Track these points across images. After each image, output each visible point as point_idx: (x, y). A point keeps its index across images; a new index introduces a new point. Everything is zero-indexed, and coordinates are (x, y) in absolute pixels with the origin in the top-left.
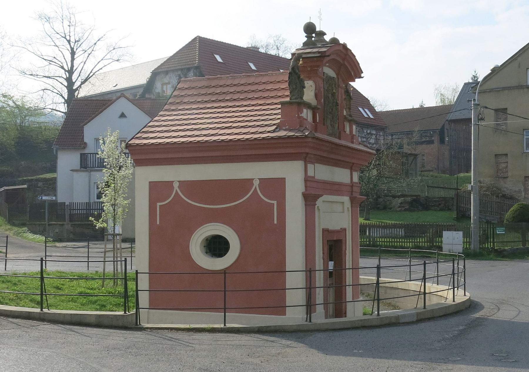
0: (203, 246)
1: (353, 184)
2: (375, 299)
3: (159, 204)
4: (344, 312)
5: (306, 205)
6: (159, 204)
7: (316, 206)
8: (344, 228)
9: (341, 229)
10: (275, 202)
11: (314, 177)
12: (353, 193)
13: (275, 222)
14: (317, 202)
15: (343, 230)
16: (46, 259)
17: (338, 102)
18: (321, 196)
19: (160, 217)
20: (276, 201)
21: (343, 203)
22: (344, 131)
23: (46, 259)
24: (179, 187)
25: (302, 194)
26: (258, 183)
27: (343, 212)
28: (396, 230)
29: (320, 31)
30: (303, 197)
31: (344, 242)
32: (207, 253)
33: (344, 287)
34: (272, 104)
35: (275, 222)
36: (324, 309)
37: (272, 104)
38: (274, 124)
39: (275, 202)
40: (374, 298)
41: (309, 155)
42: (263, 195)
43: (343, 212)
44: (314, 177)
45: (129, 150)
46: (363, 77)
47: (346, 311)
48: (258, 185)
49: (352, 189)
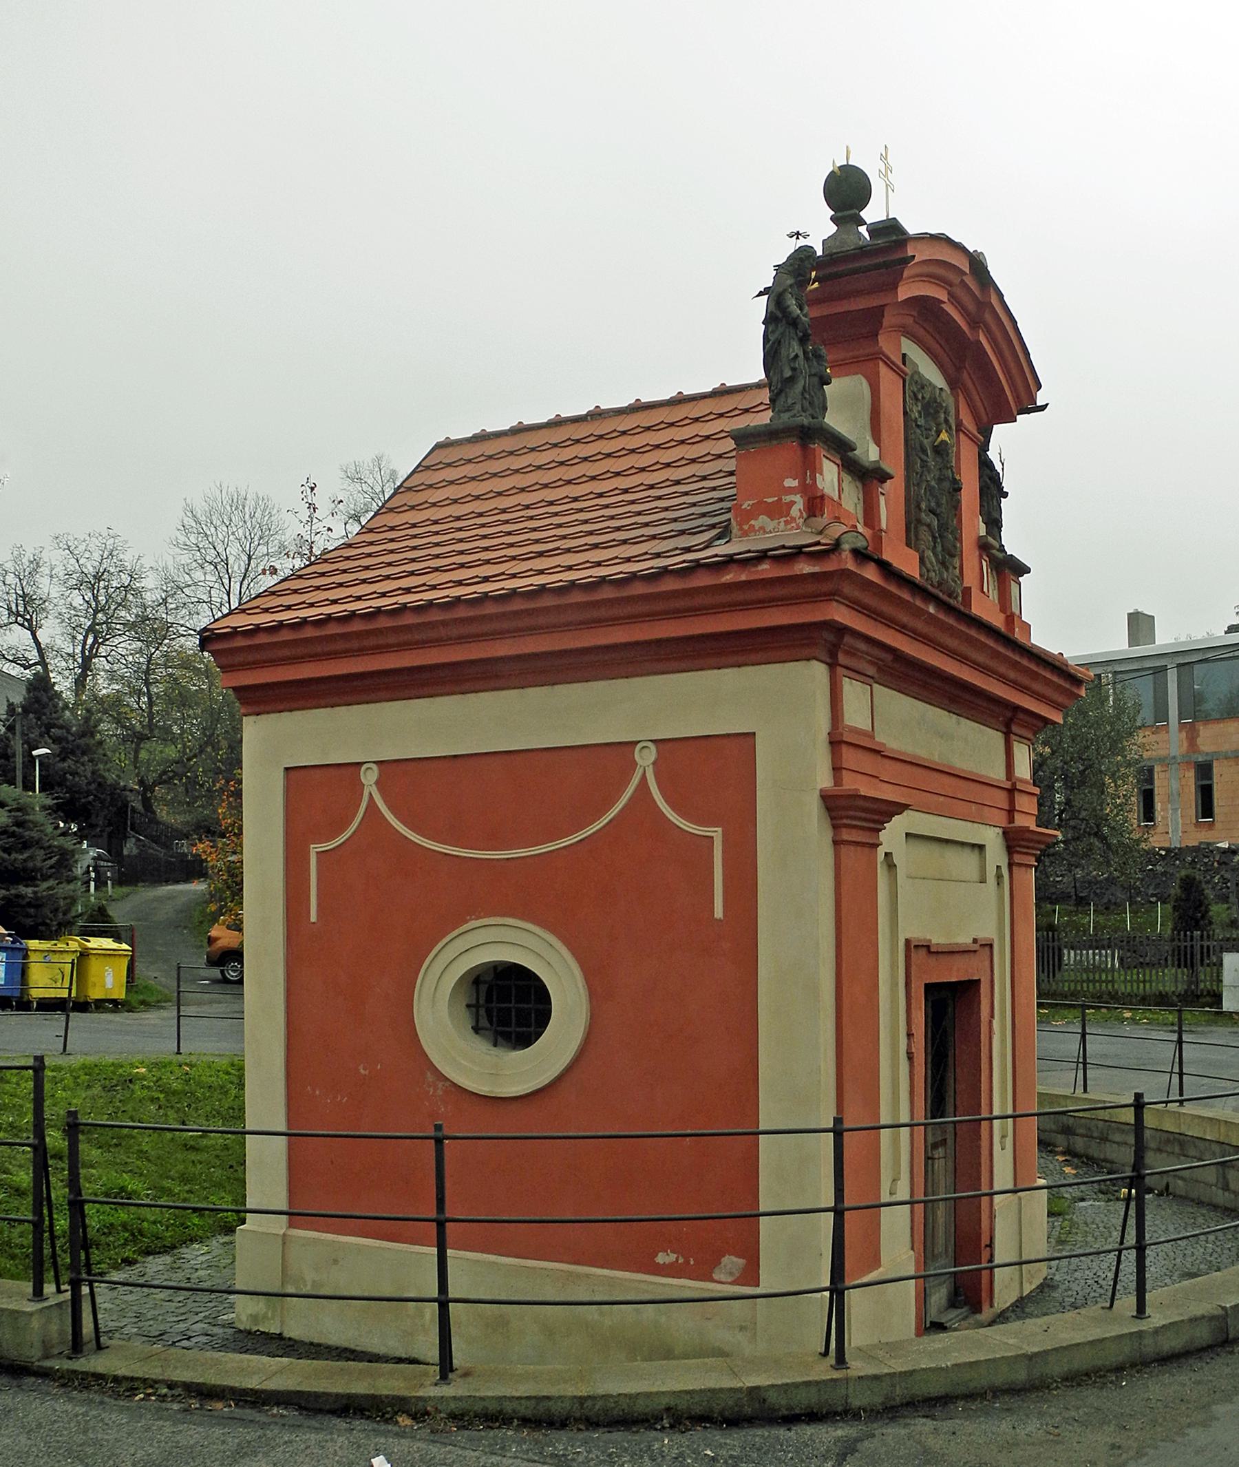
0: (464, 1004)
1: (1014, 784)
2: (1126, 1244)
3: (315, 849)
4: (985, 1240)
5: (836, 843)
6: (315, 849)
7: (881, 852)
8: (985, 939)
9: (975, 941)
10: (717, 833)
11: (870, 735)
12: (1017, 816)
13: (719, 913)
14: (883, 835)
15: (982, 945)
16: (1181, 1095)
17: (958, 478)
18: (901, 808)
19: (319, 905)
20: (719, 829)
21: (981, 848)
22: (984, 593)
23: (1181, 1095)
24: (377, 783)
25: (821, 796)
26: (653, 759)
27: (983, 881)
28: (1154, 972)
29: (888, 220)
30: (823, 810)
31: (984, 989)
32: (476, 1029)
33: (985, 1200)
34: (718, 476)
35: (719, 913)
36: (912, 1249)
37: (718, 476)
38: (713, 526)
39: (717, 833)
40: (1122, 1243)
41: (847, 639)
42: (674, 808)
43: (983, 881)
44: (870, 735)
45: (213, 653)
46: (1043, 408)
47: (992, 1238)
48: (654, 763)
49: (1012, 802)
